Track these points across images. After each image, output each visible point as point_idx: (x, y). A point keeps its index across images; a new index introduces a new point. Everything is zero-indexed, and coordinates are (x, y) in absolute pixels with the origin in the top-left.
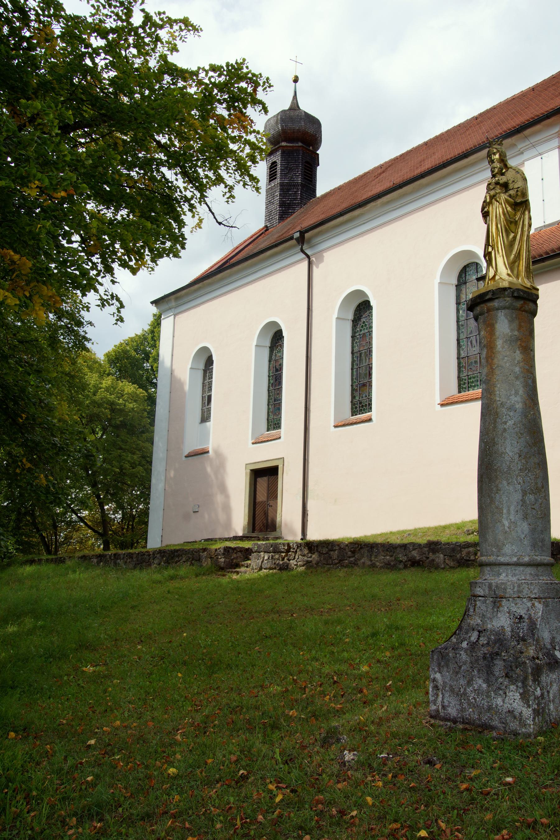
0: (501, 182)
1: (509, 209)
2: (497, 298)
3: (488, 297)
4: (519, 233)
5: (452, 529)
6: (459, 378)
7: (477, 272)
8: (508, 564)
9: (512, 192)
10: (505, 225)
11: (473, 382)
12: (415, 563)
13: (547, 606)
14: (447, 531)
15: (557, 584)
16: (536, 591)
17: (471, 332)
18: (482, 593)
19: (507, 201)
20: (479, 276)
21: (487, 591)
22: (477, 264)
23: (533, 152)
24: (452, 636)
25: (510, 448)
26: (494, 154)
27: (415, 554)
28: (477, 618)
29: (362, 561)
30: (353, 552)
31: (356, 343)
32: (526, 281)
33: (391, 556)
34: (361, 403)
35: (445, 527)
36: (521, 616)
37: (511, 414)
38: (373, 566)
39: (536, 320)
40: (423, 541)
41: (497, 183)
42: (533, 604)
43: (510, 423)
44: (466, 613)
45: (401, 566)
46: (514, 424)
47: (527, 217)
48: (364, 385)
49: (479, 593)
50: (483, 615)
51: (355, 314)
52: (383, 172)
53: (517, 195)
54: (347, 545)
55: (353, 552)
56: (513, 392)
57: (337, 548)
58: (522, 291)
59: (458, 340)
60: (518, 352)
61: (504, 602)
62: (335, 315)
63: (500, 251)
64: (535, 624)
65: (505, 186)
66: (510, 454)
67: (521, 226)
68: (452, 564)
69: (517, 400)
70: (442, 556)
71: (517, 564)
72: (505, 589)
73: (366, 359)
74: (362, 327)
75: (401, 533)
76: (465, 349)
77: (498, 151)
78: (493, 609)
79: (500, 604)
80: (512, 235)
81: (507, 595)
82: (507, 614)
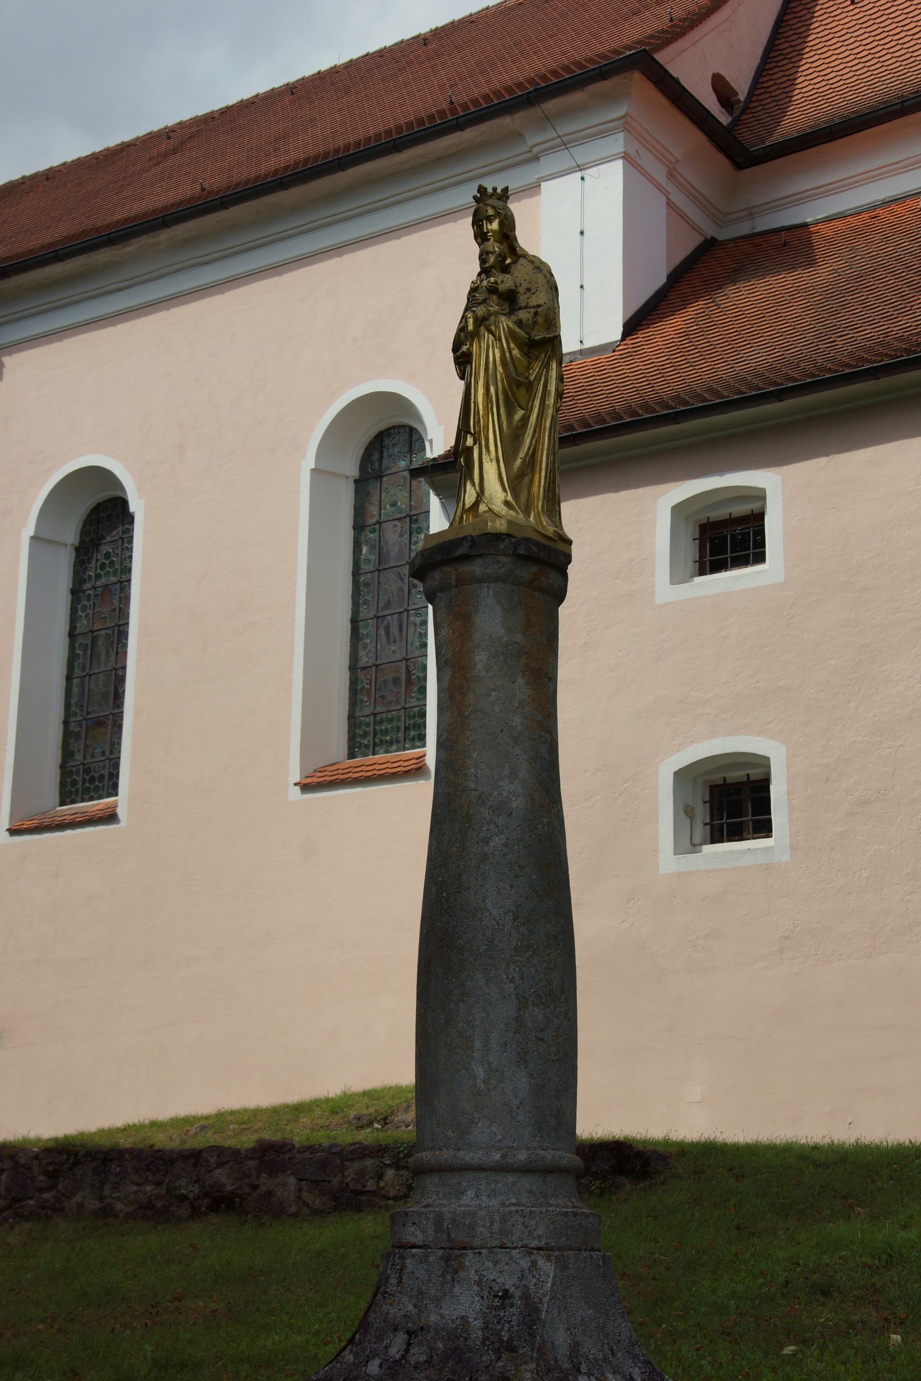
0: (502, 288)
1: (516, 352)
2: (480, 556)
3: (459, 552)
4: (536, 410)
5: (318, 1112)
6: (352, 719)
7: (411, 451)
8: (481, 1169)
9: (523, 315)
10: (504, 390)
11: (386, 732)
12: (220, 1203)
13: (564, 1267)
14: (305, 1120)
15: (587, 1216)
16: (540, 1231)
17: (388, 604)
18: (418, 1239)
19: (511, 334)
20: (417, 463)
21: (431, 1233)
22: (412, 430)
23: (562, 159)
24: (344, 1348)
25: (494, 899)
26: (490, 219)
27: (222, 1177)
28: (405, 1299)
29: (78, 1199)
30: (53, 1176)
31: (84, 608)
32: (545, 520)
33: (159, 1184)
34: (87, 771)
35: (299, 1109)
36: (506, 1292)
37: (501, 821)
38: (106, 1212)
39: (563, 611)
40: (247, 1141)
41: (492, 290)
42: (534, 1264)
43: (497, 841)
44: (380, 1291)
45: (183, 1211)
46: (505, 845)
47: (554, 374)
48: (99, 723)
49: (412, 1240)
50: (420, 1292)
51: (84, 532)
52: (174, 151)
53: (535, 323)
54: (36, 1157)
55: (53, 1176)
56: (506, 772)
57: (7, 1164)
58: (537, 543)
59: (355, 622)
60: (521, 681)
61: (470, 1259)
62: (29, 530)
63: (492, 448)
64: (537, 1311)
65: (510, 299)
66: (495, 912)
67: (539, 395)
68: (318, 1203)
69: (514, 791)
70: (292, 1181)
71: (501, 1169)
72: (472, 1227)
73: (108, 655)
74: (103, 566)
75: (178, 1123)
76: (371, 647)
77: (497, 214)
78: (443, 1276)
79: (461, 1263)
80: (520, 413)
81: (477, 1242)
82: (476, 1288)
